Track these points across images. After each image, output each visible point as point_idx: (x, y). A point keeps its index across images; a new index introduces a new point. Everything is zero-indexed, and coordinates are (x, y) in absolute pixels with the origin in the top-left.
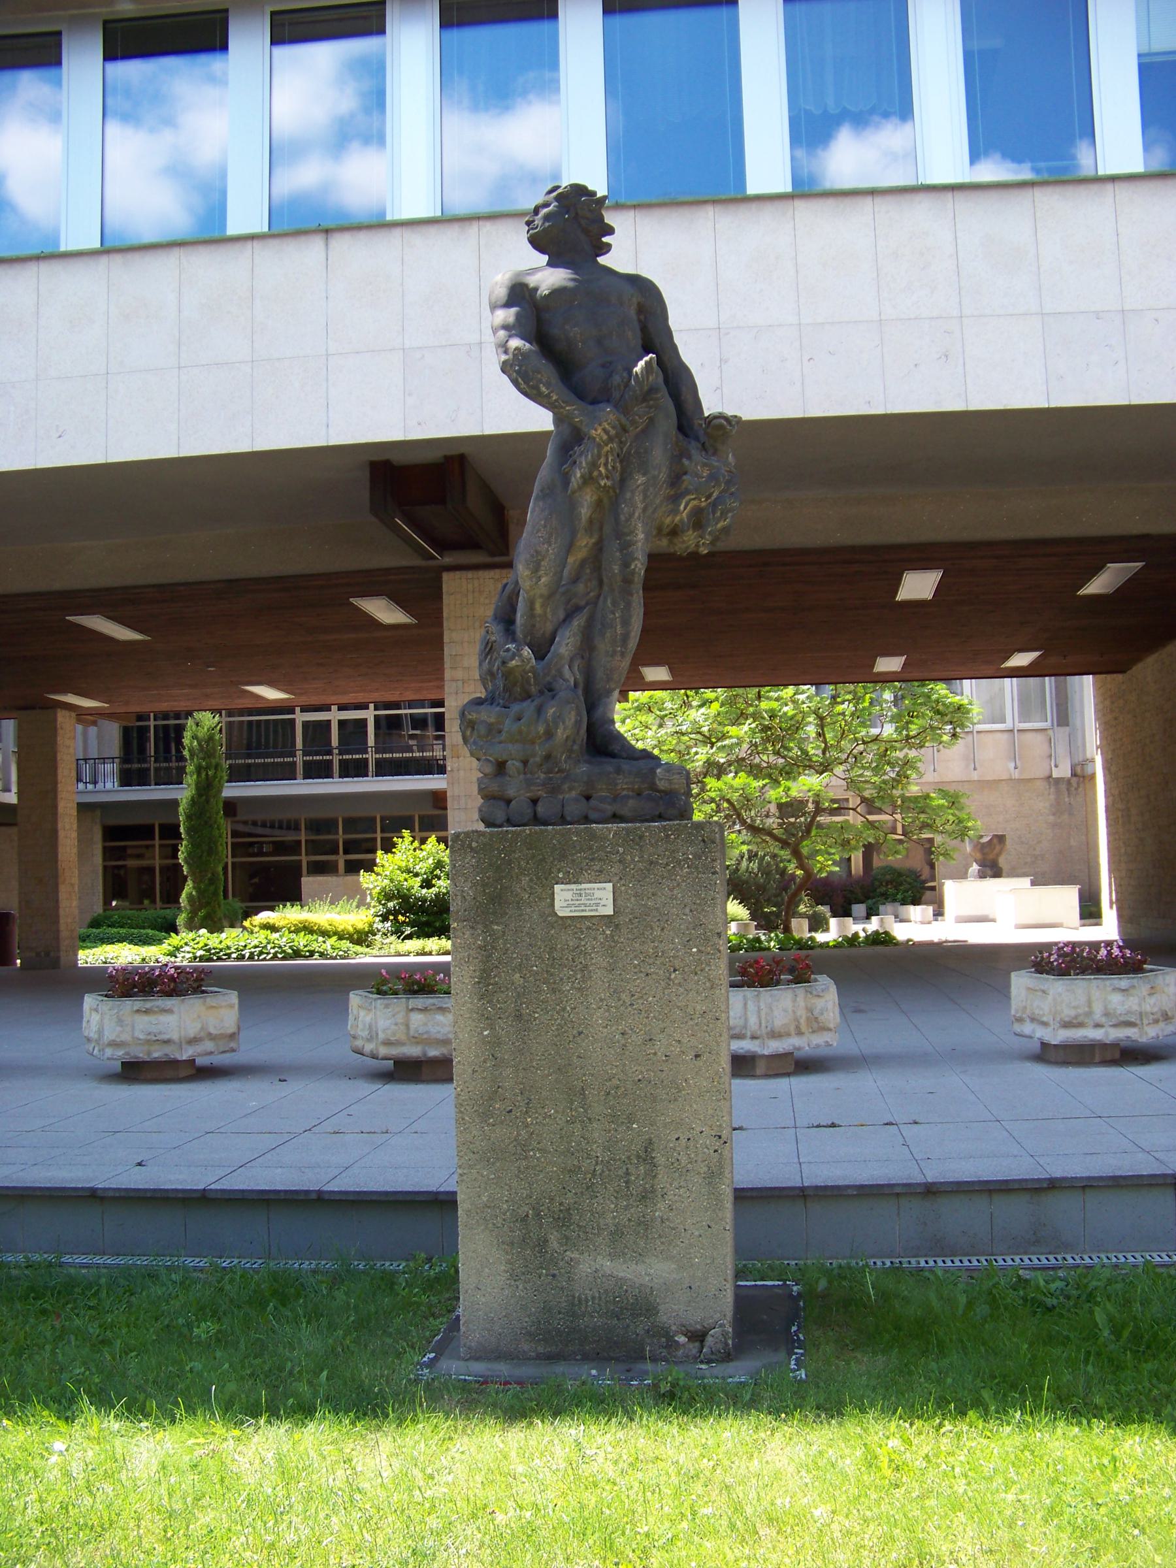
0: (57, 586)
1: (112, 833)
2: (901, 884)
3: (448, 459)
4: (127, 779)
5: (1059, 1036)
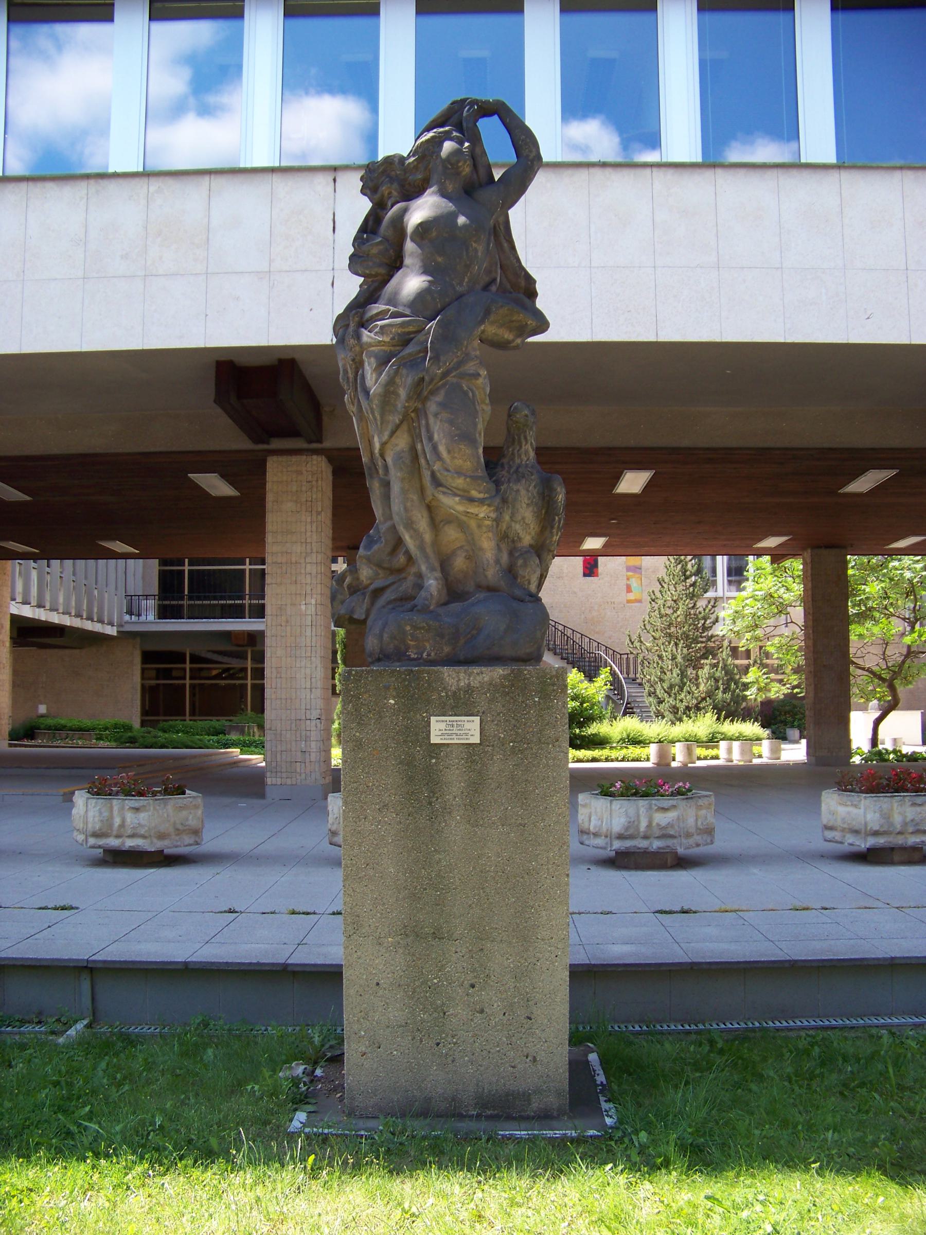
0: (686, 443)
1: (148, 657)
2: (796, 714)
3: (281, 362)
4: (164, 613)
5: (863, 844)
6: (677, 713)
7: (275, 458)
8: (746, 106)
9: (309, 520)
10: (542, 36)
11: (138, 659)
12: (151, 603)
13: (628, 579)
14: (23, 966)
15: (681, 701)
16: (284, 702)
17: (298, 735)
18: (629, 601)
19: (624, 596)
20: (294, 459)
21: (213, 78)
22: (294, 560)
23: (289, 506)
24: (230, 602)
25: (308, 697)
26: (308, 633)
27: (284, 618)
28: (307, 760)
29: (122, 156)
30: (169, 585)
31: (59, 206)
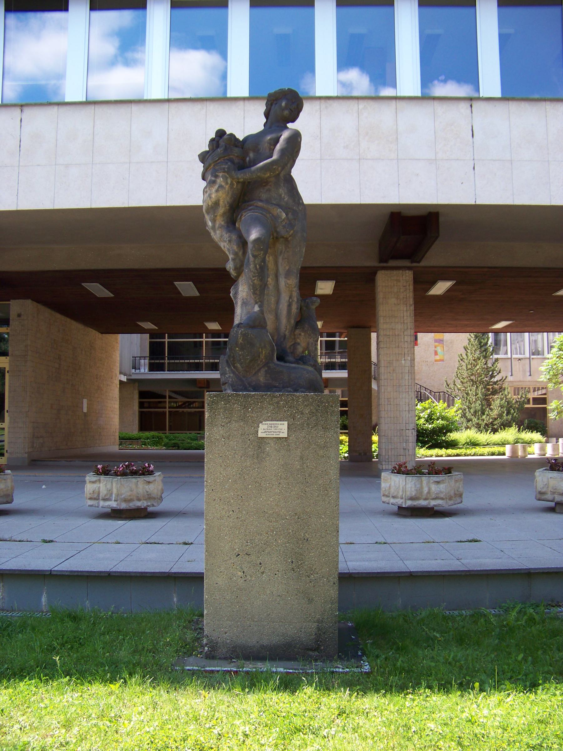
1: (142, 395)
3: (430, 214)
6: (480, 427)
7: (383, 272)
8: (449, 60)
9: (405, 309)
10: (325, 21)
11: (136, 396)
12: (147, 361)
13: (435, 347)
14: (543, 573)
15: (483, 420)
16: (393, 419)
17: (401, 439)
18: (436, 361)
19: (433, 358)
20: (395, 272)
21: (130, 44)
22: (397, 334)
23: (393, 301)
24: (187, 361)
25: (407, 416)
26: (407, 378)
27: (391, 368)
28: (407, 454)
29: (73, 92)
30: (156, 351)
31: (39, 120)
